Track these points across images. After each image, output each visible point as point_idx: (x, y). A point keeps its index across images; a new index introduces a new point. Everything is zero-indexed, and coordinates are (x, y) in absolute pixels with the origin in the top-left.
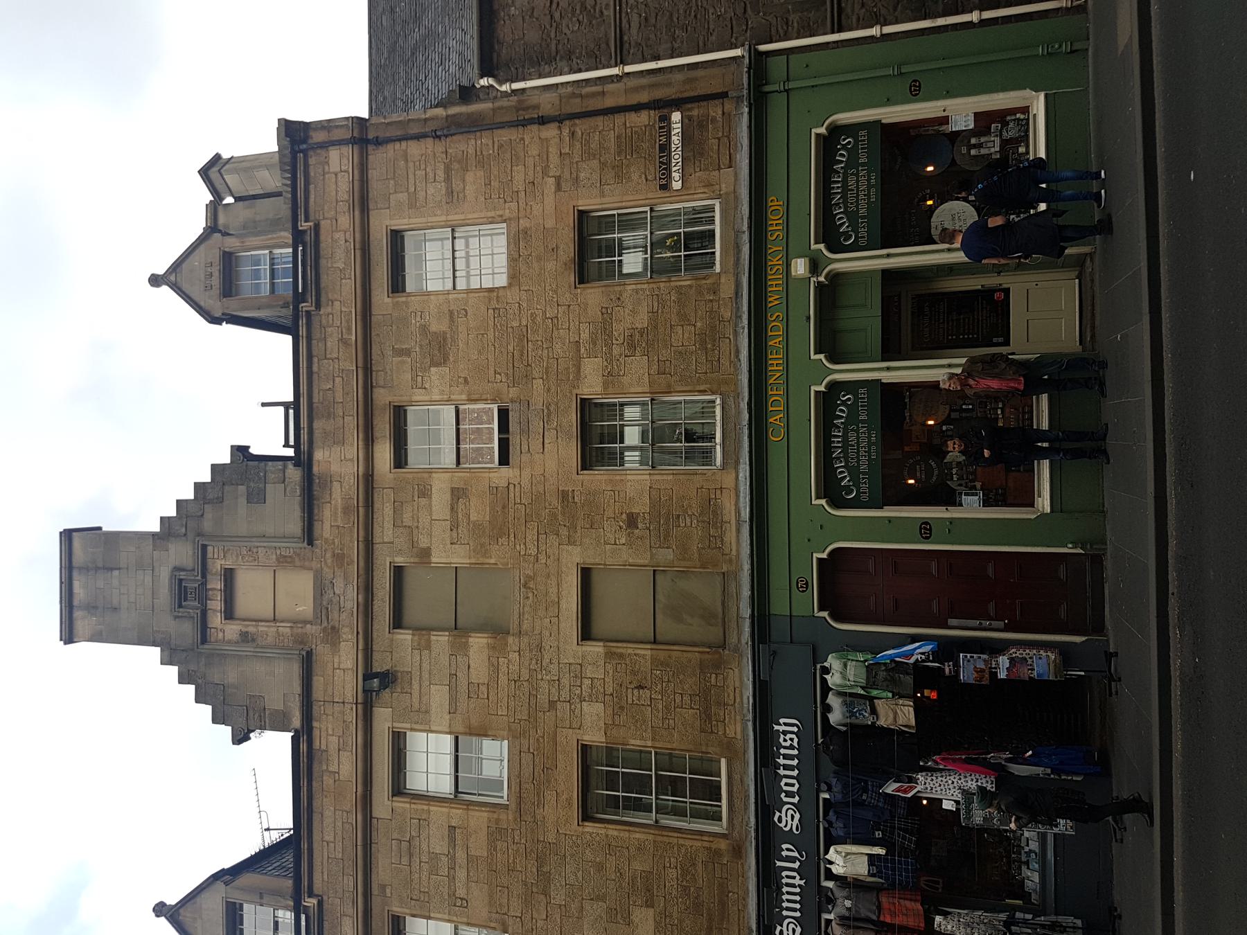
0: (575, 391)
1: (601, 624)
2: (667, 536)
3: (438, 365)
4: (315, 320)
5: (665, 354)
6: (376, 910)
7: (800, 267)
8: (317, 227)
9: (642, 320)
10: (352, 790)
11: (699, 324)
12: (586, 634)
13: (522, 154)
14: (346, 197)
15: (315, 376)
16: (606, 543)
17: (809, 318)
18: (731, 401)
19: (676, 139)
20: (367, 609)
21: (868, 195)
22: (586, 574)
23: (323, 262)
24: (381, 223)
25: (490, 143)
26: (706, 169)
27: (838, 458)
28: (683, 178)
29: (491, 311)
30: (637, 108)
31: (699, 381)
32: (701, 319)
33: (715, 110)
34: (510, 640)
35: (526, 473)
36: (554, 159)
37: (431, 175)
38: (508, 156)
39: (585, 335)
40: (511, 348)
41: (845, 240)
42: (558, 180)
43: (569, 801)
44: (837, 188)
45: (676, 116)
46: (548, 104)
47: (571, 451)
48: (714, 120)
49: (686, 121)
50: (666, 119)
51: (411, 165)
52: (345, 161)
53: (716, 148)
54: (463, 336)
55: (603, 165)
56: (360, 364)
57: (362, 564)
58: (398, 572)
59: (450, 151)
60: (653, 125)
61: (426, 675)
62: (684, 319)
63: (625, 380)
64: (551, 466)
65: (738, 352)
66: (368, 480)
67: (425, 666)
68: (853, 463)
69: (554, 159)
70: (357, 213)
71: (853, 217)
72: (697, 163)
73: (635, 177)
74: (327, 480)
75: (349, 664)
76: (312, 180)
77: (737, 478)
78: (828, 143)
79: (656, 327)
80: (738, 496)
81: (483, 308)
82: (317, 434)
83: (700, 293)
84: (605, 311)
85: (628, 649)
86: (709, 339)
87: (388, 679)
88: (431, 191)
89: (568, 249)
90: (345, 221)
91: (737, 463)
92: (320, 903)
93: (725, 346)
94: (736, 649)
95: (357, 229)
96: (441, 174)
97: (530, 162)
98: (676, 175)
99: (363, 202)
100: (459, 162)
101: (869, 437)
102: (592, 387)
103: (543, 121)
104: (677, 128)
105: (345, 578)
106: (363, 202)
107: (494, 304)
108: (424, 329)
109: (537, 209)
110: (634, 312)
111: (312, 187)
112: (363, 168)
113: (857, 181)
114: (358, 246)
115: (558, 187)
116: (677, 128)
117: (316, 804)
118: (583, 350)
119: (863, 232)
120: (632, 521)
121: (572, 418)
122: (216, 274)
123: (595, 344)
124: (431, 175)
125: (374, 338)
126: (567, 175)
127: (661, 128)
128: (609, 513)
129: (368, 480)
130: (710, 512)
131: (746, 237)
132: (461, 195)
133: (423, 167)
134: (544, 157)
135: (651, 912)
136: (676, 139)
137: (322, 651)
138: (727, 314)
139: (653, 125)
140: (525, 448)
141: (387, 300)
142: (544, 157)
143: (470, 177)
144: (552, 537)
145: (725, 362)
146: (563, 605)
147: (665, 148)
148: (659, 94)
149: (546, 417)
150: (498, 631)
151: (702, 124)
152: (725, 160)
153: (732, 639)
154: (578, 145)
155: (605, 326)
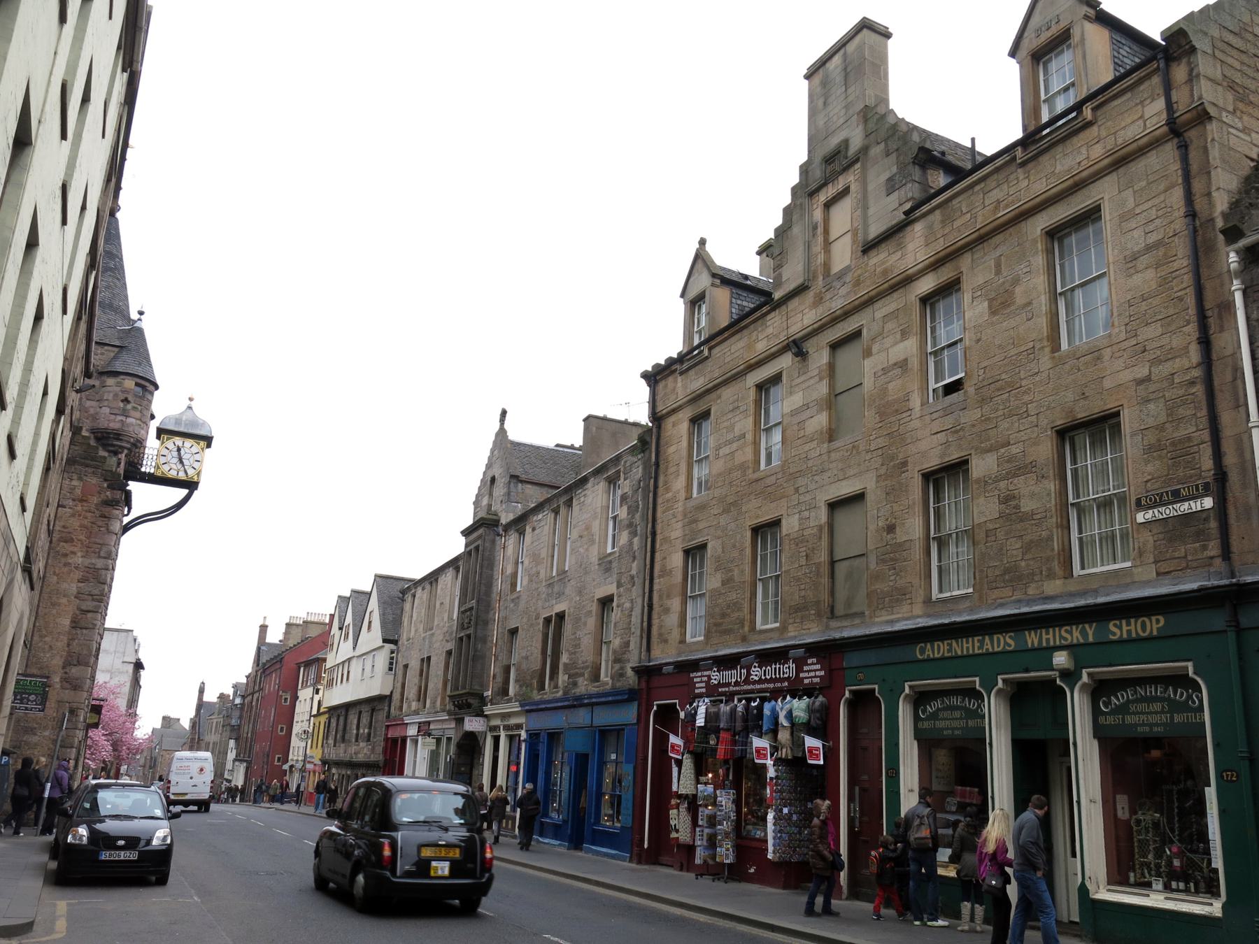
0: (973, 452)
1: (842, 517)
2: (884, 561)
3: (990, 307)
4: (1013, 167)
5: (1001, 535)
6: (708, 398)
7: (1061, 659)
8: (1089, 124)
9: (1027, 506)
10: (751, 356)
11: (1023, 564)
12: (833, 506)
13: (1173, 327)
14: (1120, 141)
15: (970, 192)
16: (878, 510)
17: (1027, 671)
18: (967, 604)
19: (1184, 507)
20: (835, 320)
21: (1143, 725)
22: (859, 498)
23: (1060, 148)
24: (1105, 192)
25: (1184, 285)
26: (1155, 547)
27: (1136, 692)
28: (1148, 523)
29: (1031, 344)
30: (1218, 455)
31: (981, 571)
32: (1028, 565)
33: (1214, 548)
34: (826, 445)
35: (916, 424)
36: (1166, 368)
37: (1151, 227)
38: (1171, 311)
39: (1015, 450)
40: (1003, 376)
41: (1104, 703)
42: (1147, 379)
43: (757, 517)
44: (1151, 691)
45: (1208, 502)
46: (1220, 342)
47: (933, 462)
48: (1204, 548)
49: (1204, 515)
50: (1207, 490)
51: (1162, 198)
52: (1155, 120)
53: (1177, 554)
54: (1012, 323)
55: (1161, 428)
56: (982, 231)
57: (857, 303)
58: (857, 334)
59: (1176, 239)
60: (1200, 477)
61: (807, 384)
62: (1027, 548)
63: (982, 500)
64: (923, 445)
65: (1002, 605)
66: (907, 281)
67: (812, 382)
68: (1132, 708)
69: (1166, 368)
70: (1106, 162)
71: (1123, 709)
72: (1161, 536)
73: (1150, 468)
74: (901, 246)
75: (807, 322)
76: (1136, 90)
77: (919, 617)
78: (1181, 680)
79: (1022, 521)
80: (907, 619)
81: (1034, 336)
82: (931, 218)
83: (1048, 559)
84: (1033, 464)
85: (824, 543)
86: (1014, 577)
87: (801, 354)
88: (1136, 234)
89: (1083, 412)
90: (1098, 151)
91: (929, 616)
92: (707, 358)
93: (1007, 592)
94: (827, 627)
95: (1038, 200)
96: (1153, 238)
97: (1165, 340)
98: (1149, 515)
99: (1121, 161)
100: (1165, 254)
101: (1157, 725)
102: (981, 467)
103: (1205, 342)
104: (1195, 506)
105: (848, 293)
106: (1121, 161)
107: (1038, 346)
108: (1016, 281)
109: (1119, 364)
110: (1032, 495)
111: (1129, 95)
112: (1154, 144)
113: (1156, 713)
114: (1076, 178)
115: (1140, 382)
116: (1195, 506)
117: (745, 332)
118: (1003, 450)
119: (1110, 720)
120: (891, 529)
121: (954, 455)
122: (1049, 34)
123: (1008, 461)
124: (1151, 227)
125: (1008, 232)
126: (1152, 388)
127: (1197, 486)
128: (896, 507)
129: (907, 281)
130: (900, 596)
131: (1090, 601)
132: (1132, 271)
133: (1160, 213)
134: (1171, 355)
135: (719, 584)
136: (1184, 507)
137: (809, 296)
138: (1031, 591)
139: (1200, 477)
140: (935, 416)
141: (1039, 230)
142: (1171, 355)
143: (1150, 274)
144: (880, 460)
145: (996, 593)
146: (844, 483)
147: (1177, 497)
148: (1234, 477)
149: (955, 430)
150: (831, 435)
151: (1200, 535)
152: (1164, 567)
153: (833, 624)
154: (1181, 392)
155: (1021, 468)
